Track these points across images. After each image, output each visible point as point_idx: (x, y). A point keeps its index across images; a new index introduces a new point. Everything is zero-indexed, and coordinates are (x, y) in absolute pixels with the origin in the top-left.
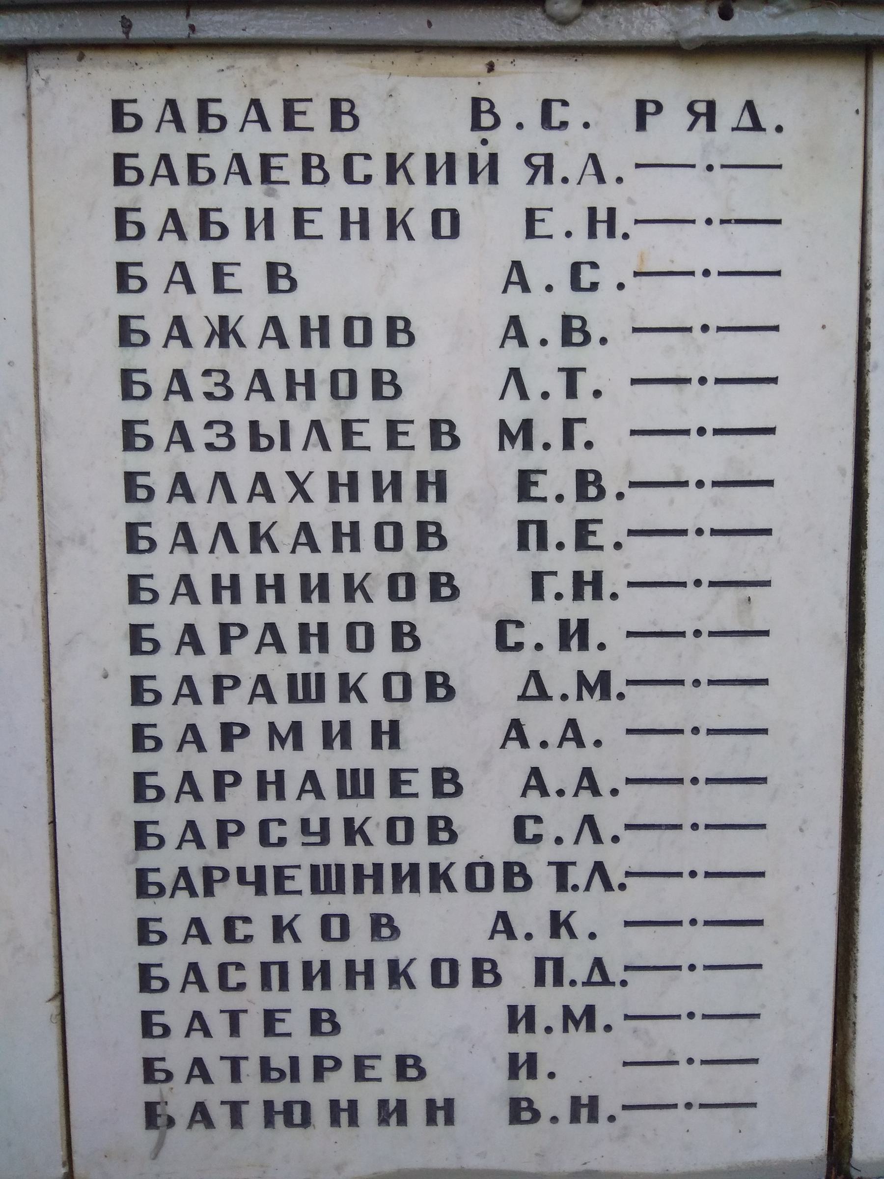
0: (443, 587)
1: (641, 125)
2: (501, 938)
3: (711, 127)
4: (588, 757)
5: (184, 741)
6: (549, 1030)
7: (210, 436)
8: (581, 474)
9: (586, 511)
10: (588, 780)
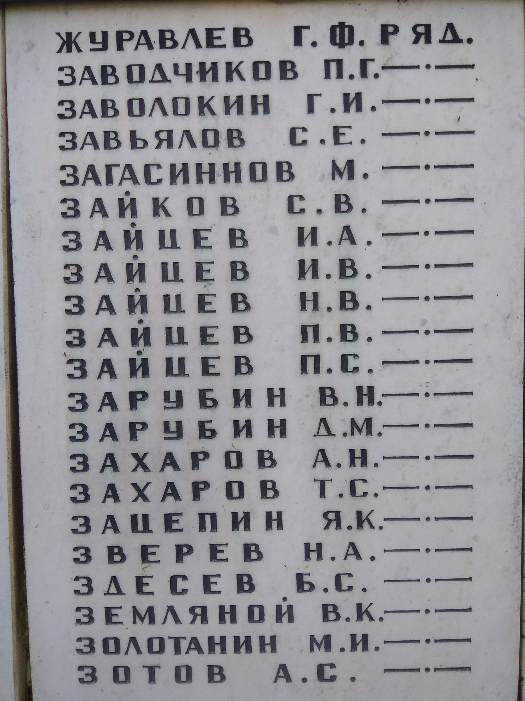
3: (428, 41)
5: (104, 436)
6: (329, 309)
9: (349, 348)
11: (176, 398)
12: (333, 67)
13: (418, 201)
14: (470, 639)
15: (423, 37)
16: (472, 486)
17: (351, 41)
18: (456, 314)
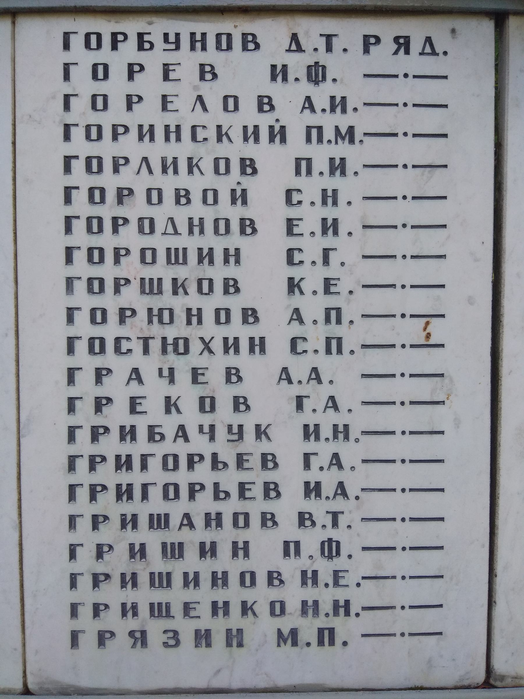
0: (268, 520)
1: (366, 51)
3: (407, 52)
4: (344, 476)
10: (341, 489)
11: (119, 169)
12: (314, 132)
13: (395, 198)
14: (447, 135)
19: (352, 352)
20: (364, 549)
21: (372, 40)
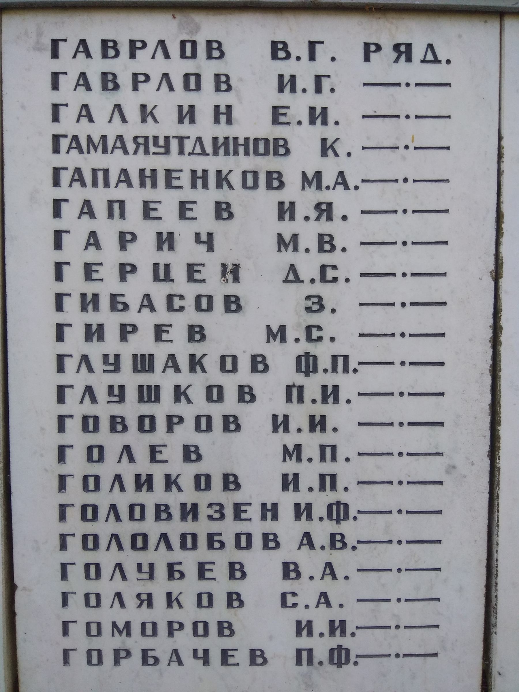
1: (367, 59)
2: (305, 548)
3: (409, 59)
6: (307, 250)
7: (211, 512)
8: (321, 236)
9: (327, 259)
15: (403, 57)
16: (447, 242)
17: (347, 661)
18: (427, 379)
19: (347, 460)
20: (360, 394)
21: (373, 48)
